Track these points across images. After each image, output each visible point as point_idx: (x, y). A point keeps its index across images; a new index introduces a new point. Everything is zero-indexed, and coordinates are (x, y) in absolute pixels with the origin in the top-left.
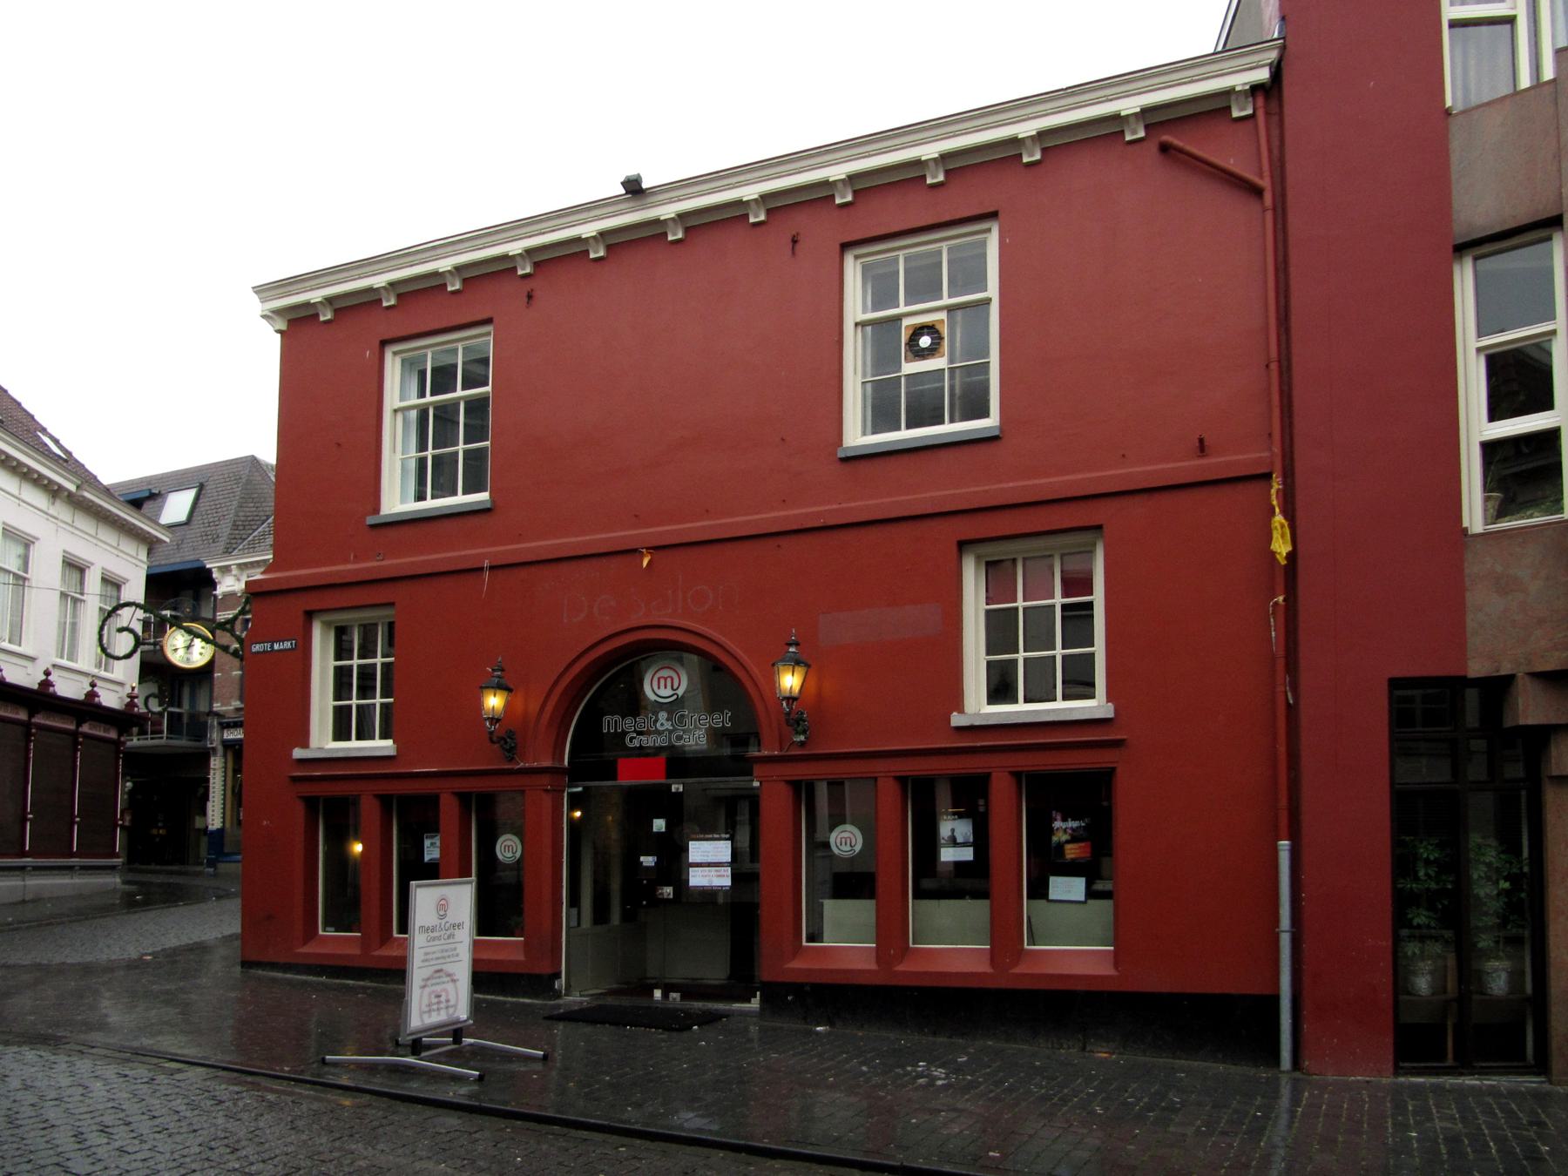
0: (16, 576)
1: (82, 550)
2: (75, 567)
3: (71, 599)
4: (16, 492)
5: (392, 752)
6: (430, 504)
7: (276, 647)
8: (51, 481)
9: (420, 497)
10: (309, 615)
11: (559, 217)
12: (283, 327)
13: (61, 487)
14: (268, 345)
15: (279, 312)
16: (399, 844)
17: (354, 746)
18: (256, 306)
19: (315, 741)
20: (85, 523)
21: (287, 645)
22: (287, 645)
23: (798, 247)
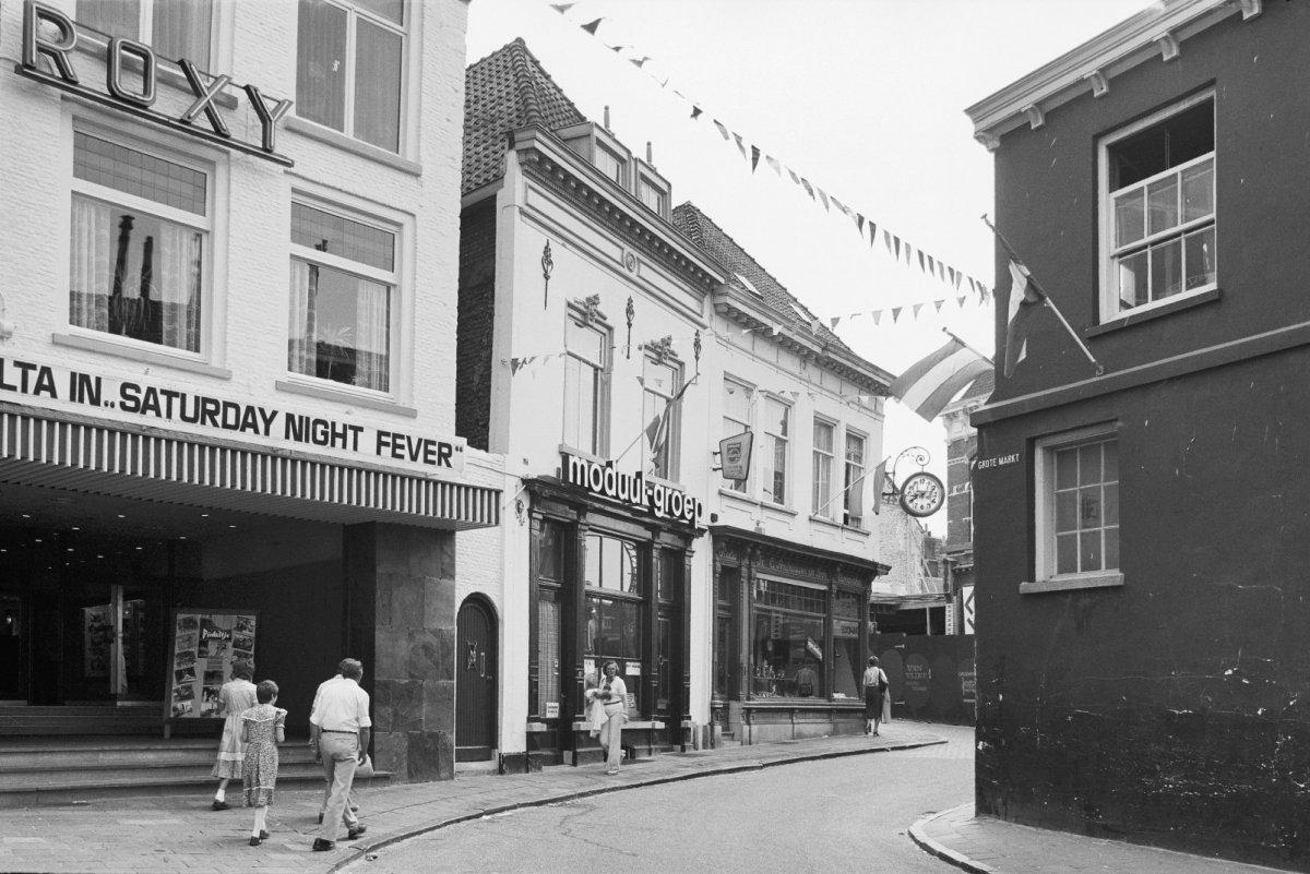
0: (778, 439)
1: (830, 408)
2: (824, 426)
3: (822, 460)
4: (774, 360)
5: (1119, 582)
6: (1151, 305)
7: (1001, 462)
8: (803, 347)
9: (1141, 298)
10: (1031, 444)
11: (1113, 35)
12: (997, 144)
13: (811, 352)
14: (982, 163)
15: (990, 130)
16: (1107, 544)
17: (1080, 578)
18: (968, 126)
19: (1040, 574)
20: (831, 382)
21: (1011, 459)
22: (1011, 459)
23: (545, 244)
